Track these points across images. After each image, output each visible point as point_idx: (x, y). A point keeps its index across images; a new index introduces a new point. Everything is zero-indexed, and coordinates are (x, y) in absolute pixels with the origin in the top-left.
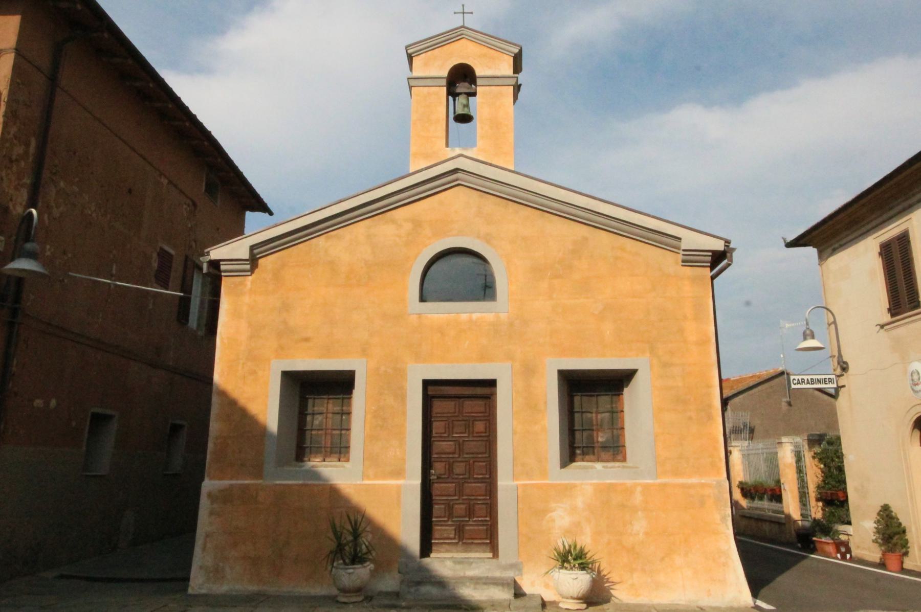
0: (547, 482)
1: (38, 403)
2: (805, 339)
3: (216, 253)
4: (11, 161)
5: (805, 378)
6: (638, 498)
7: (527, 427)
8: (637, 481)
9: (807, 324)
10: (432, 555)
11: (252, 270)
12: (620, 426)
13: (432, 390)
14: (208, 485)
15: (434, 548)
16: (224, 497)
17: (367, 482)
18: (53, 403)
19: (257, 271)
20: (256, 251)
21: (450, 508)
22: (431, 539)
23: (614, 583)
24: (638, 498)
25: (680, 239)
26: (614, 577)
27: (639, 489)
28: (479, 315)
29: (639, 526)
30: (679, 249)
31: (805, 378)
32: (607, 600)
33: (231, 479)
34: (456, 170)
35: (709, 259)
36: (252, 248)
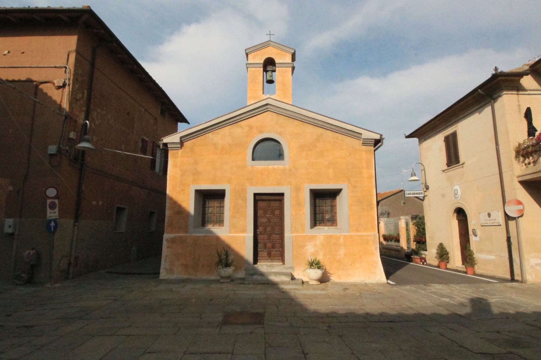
3: (166, 140)
6: (342, 241)
7: (297, 212)
14: (166, 236)
24: (342, 241)
26: (331, 272)
27: (342, 237)
33: (176, 233)
34: (267, 104)
36: (181, 138)
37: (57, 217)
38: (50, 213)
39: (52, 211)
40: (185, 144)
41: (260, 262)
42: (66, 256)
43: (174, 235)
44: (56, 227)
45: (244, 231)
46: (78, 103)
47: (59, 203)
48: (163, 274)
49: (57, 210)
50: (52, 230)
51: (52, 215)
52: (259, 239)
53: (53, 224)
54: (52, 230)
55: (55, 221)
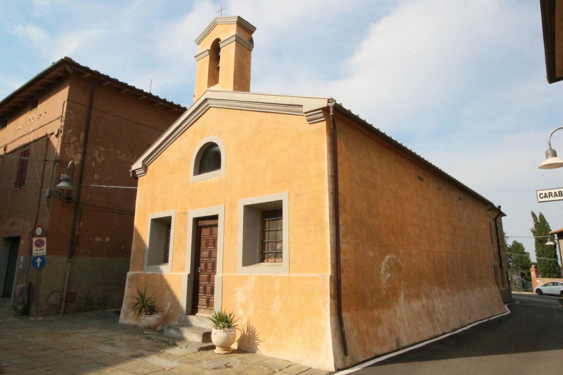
0: (236, 274)
1: (98, 239)
2: (547, 158)
3: (134, 167)
4: (70, 144)
5: (553, 191)
6: (277, 286)
7: (230, 240)
8: (278, 275)
9: (550, 145)
10: (197, 314)
11: (145, 172)
12: (280, 240)
13: (201, 223)
14: (129, 274)
15: (199, 310)
16: (133, 279)
17: (172, 273)
18: (107, 239)
19: (148, 172)
20: (146, 163)
21: (205, 288)
22: (197, 305)
23: (260, 341)
24: (277, 286)
25: (302, 106)
26: (261, 337)
27: (278, 280)
28: (214, 178)
29: (277, 305)
30: (301, 112)
31: (543, 192)
32: (254, 352)
33: (136, 271)
34: (206, 100)
35: (322, 115)
36: (144, 162)
37: (45, 254)
38: (37, 250)
39: (39, 249)
40: (150, 168)
41: (200, 313)
42: (57, 292)
43: (135, 272)
44: (42, 264)
45: (183, 269)
46: (72, 146)
47: (47, 241)
48: (123, 319)
49: (44, 247)
50: (38, 266)
51: (38, 252)
52: (201, 279)
53: (39, 260)
54: (38, 266)
55: (42, 257)
